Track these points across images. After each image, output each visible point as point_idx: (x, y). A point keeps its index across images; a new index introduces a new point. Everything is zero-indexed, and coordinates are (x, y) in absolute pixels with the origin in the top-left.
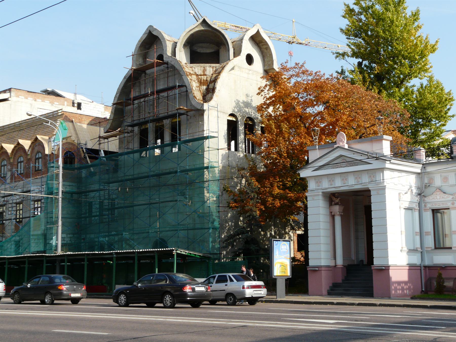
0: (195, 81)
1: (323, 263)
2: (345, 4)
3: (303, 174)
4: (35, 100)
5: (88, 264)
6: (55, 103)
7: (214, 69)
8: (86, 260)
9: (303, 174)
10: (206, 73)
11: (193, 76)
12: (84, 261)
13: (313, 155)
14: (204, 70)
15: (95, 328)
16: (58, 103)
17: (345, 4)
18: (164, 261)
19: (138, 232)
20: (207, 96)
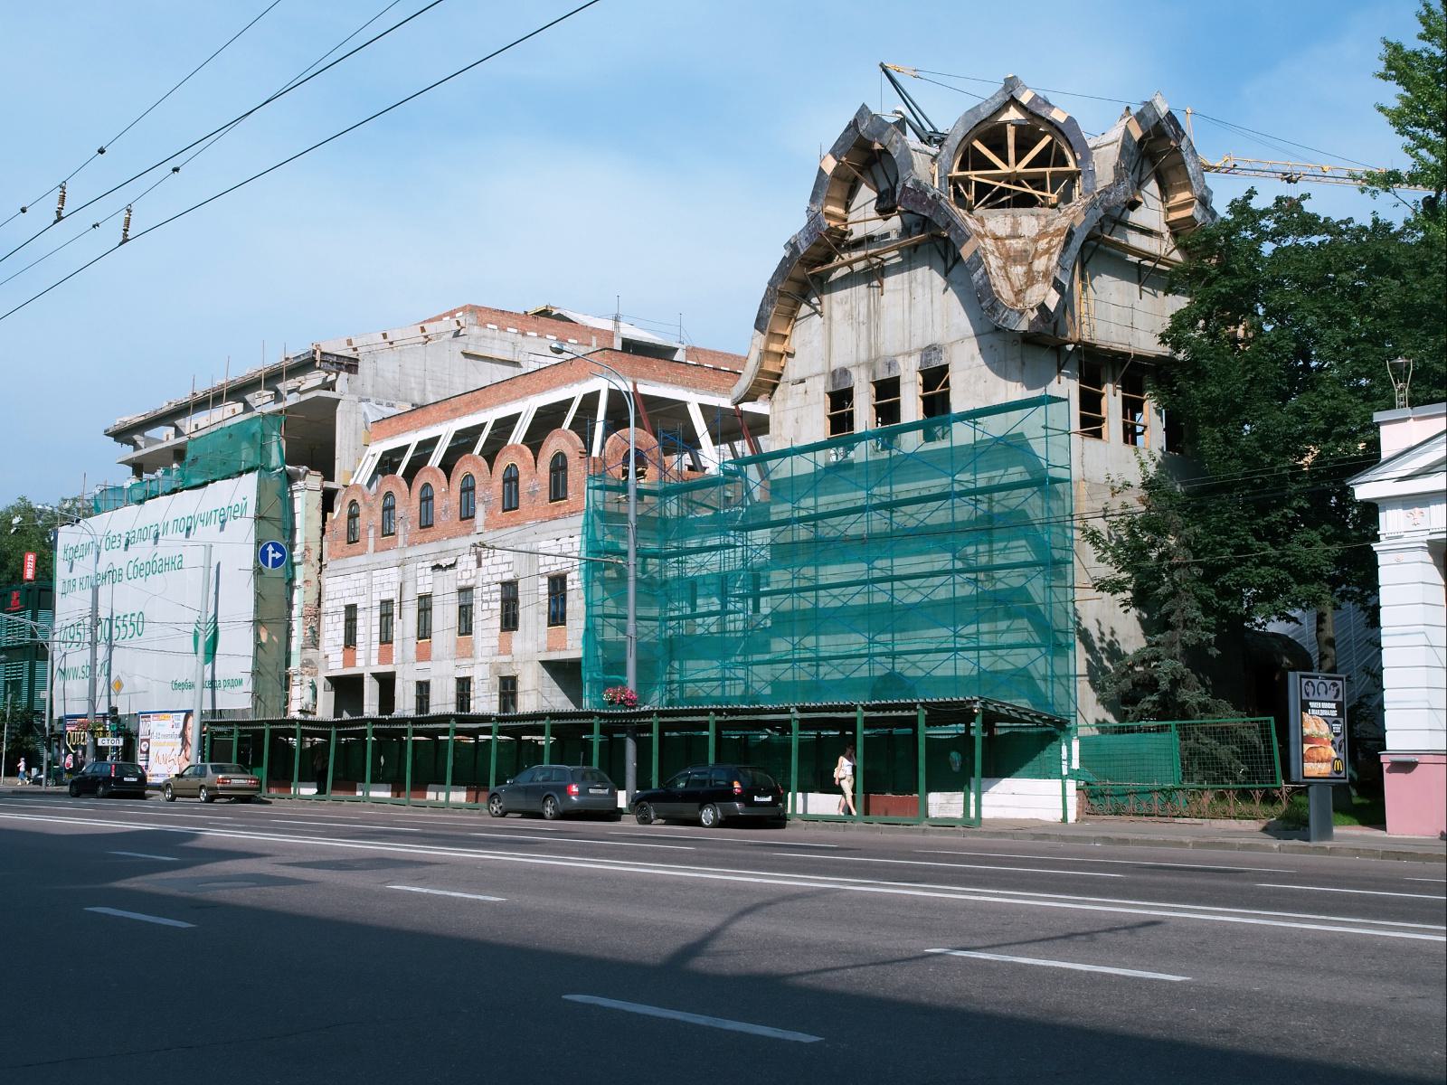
0: (993, 253)
1: (78, 708)
2: (1387, 44)
3: (1364, 490)
4: (524, 334)
5: (601, 744)
6: (570, 341)
7: (1043, 222)
8: (596, 729)
9: (1364, 490)
10: (1021, 231)
11: (986, 240)
12: (592, 733)
13: (1393, 437)
14: (1016, 225)
15: (469, 885)
16: (575, 342)
17: (1387, 44)
18: (667, 734)
19: (827, 654)
20: (1028, 292)
